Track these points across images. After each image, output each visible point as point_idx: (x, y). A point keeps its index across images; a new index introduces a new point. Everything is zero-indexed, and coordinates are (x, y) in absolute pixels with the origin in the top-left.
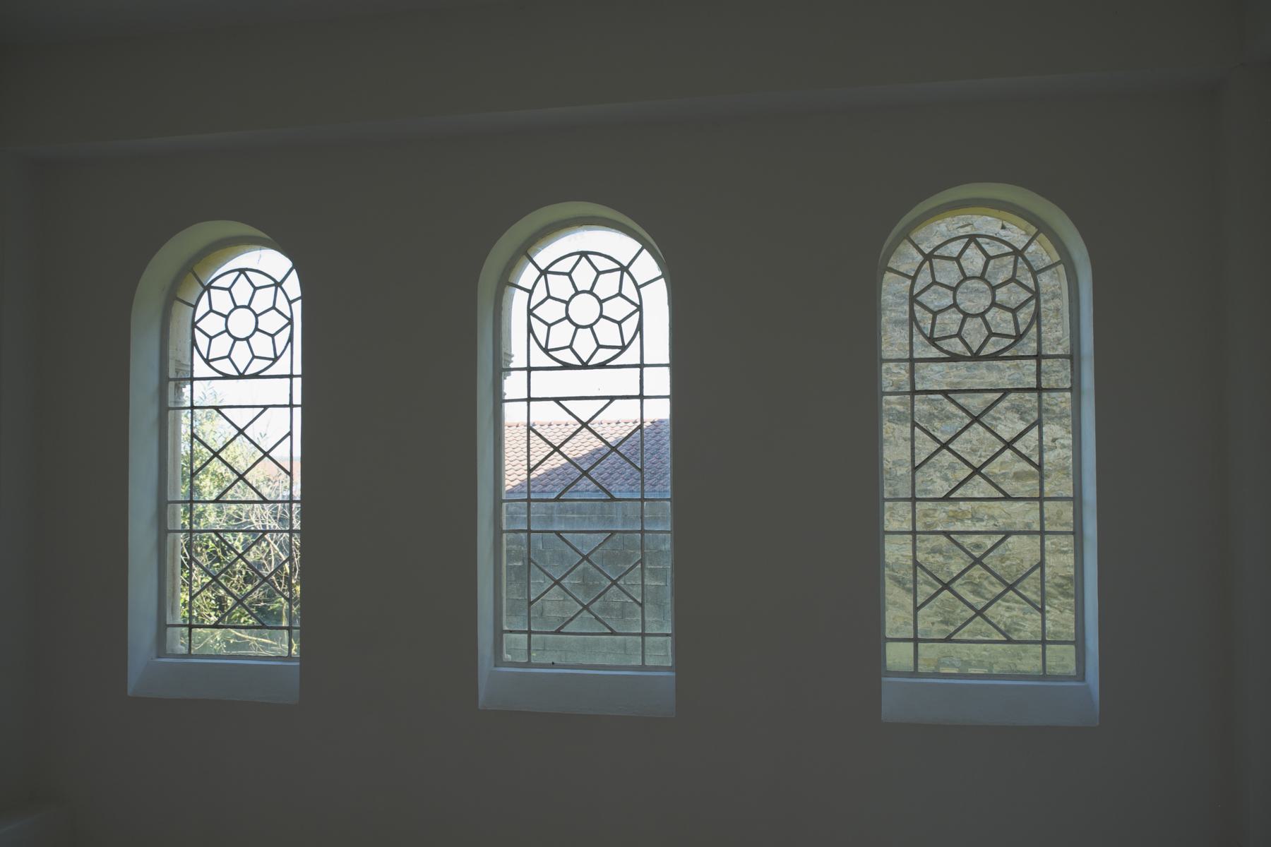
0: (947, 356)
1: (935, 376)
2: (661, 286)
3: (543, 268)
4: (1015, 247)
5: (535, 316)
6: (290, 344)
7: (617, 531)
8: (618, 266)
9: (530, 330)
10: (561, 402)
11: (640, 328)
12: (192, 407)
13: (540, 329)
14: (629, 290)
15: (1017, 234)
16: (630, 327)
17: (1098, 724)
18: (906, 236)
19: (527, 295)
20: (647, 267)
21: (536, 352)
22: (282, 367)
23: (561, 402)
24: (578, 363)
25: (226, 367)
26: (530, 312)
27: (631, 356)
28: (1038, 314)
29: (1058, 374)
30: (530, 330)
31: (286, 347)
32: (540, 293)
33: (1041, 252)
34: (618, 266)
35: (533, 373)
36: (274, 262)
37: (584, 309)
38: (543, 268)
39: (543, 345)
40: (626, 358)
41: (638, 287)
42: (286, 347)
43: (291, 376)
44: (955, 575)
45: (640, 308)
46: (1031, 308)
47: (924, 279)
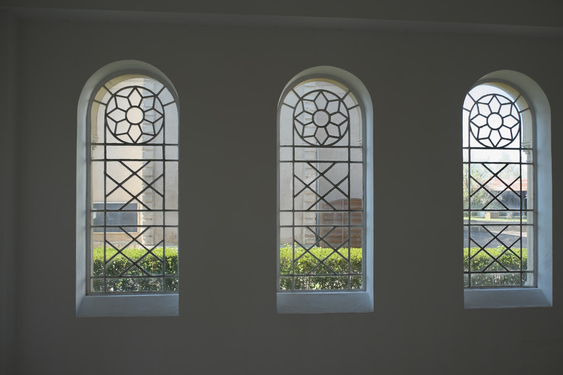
0: (310, 145)
1: (300, 154)
2: (174, 107)
3: (476, 100)
4: (339, 97)
5: (473, 123)
6: (295, 131)
7: (337, 226)
8: (152, 95)
9: (106, 124)
10: (485, 164)
11: (163, 125)
12: (470, 163)
13: (112, 124)
14: (158, 107)
15: (340, 91)
16: (343, 128)
17: (178, 315)
18: (291, 88)
19: (293, 110)
20: (167, 96)
21: (473, 140)
22: (516, 144)
23: (485, 164)
24: (131, 142)
25: (487, 143)
26: (106, 115)
27: (344, 142)
28: (349, 128)
29: (357, 155)
30: (106, 124)
31: (294, 133)
32: (112, 106)
33: (350, 101)
34: (152, 95)
35: (472, 150)
36: (478, 91)
37: (495, 121)
38: (476, 100)
39: (476, 137)
40: (341, 143)
41: (163, 106)
42: (294, 133)
43: (470, 148)
44: (295, 249)
45: (163, 116)
46: (517, 127)
47: (299, 109)
